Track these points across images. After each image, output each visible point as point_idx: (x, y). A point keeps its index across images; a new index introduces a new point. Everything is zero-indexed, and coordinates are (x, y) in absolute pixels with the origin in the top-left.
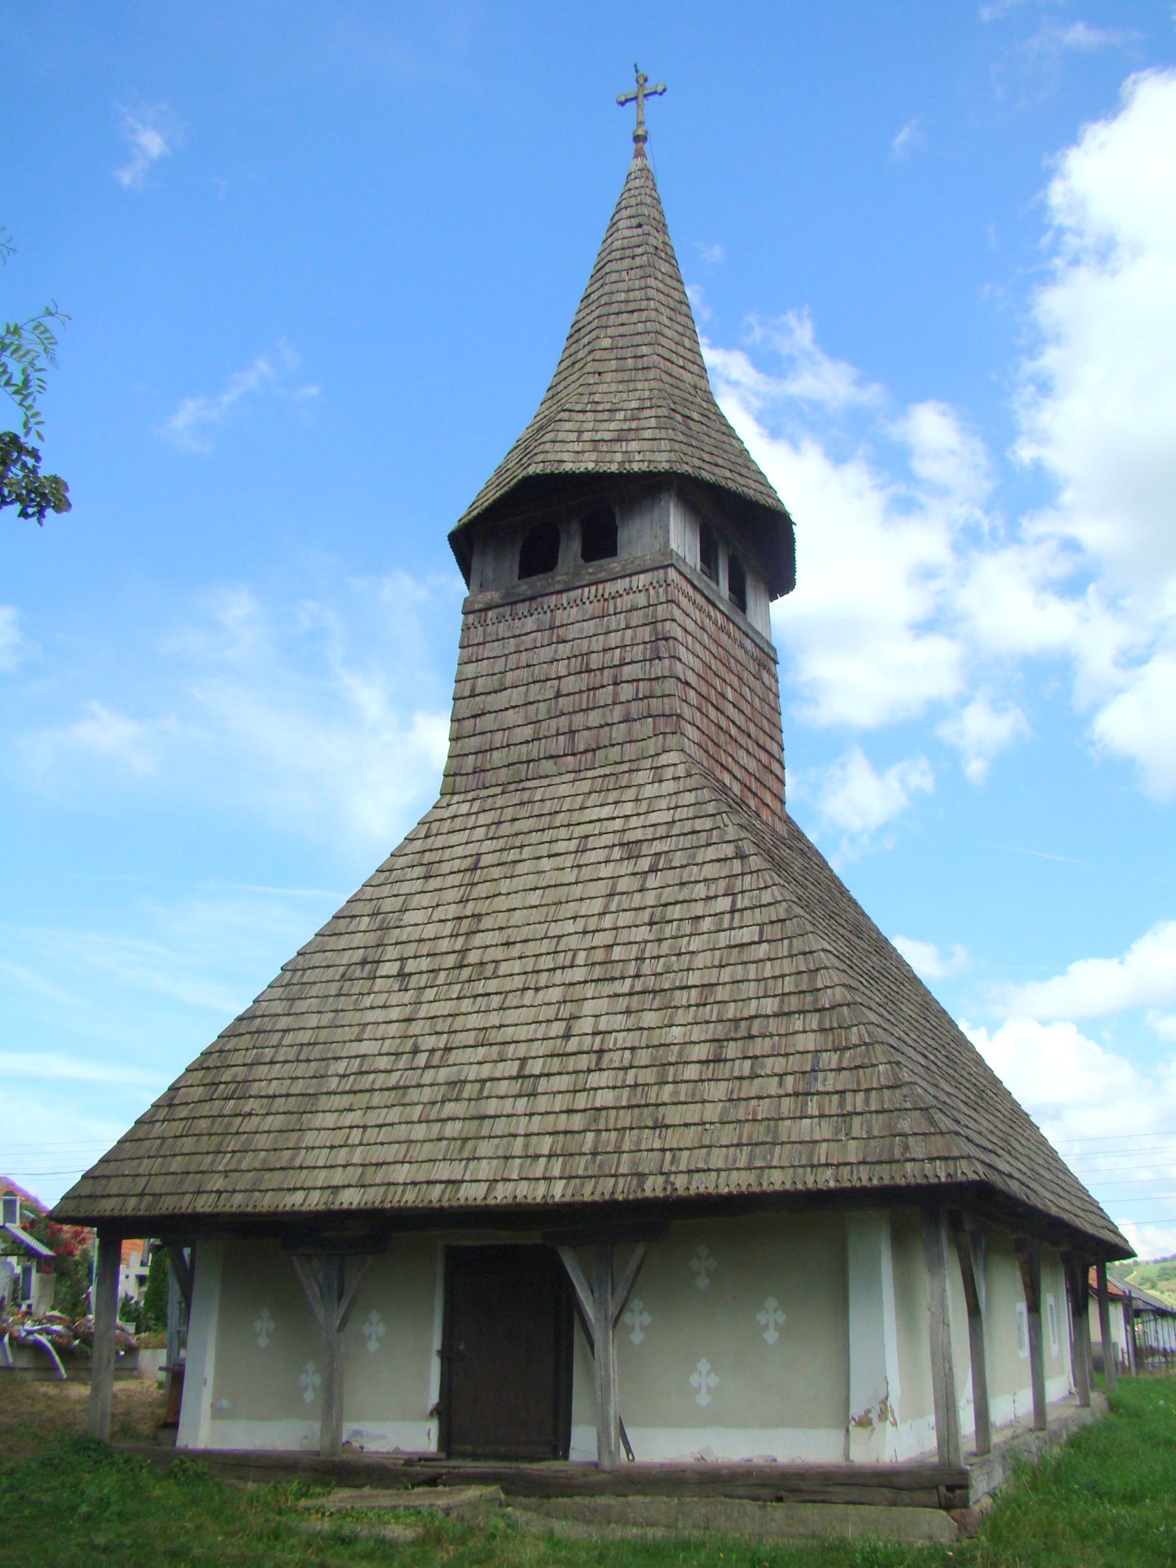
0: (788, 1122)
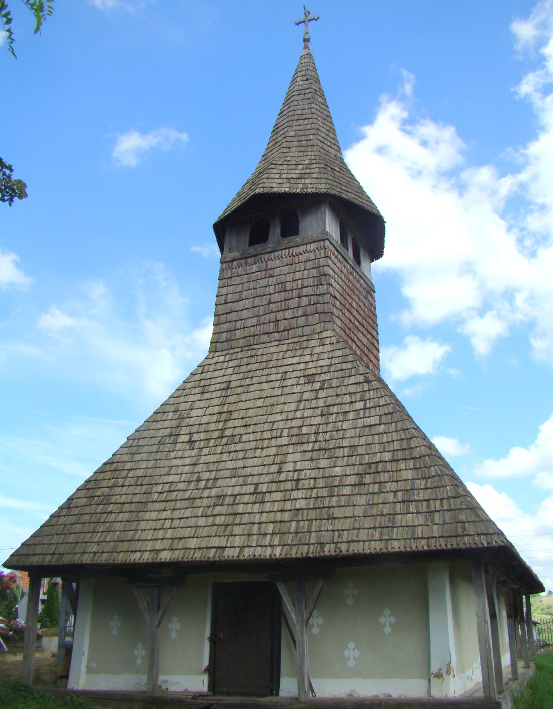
0: (400, 516)
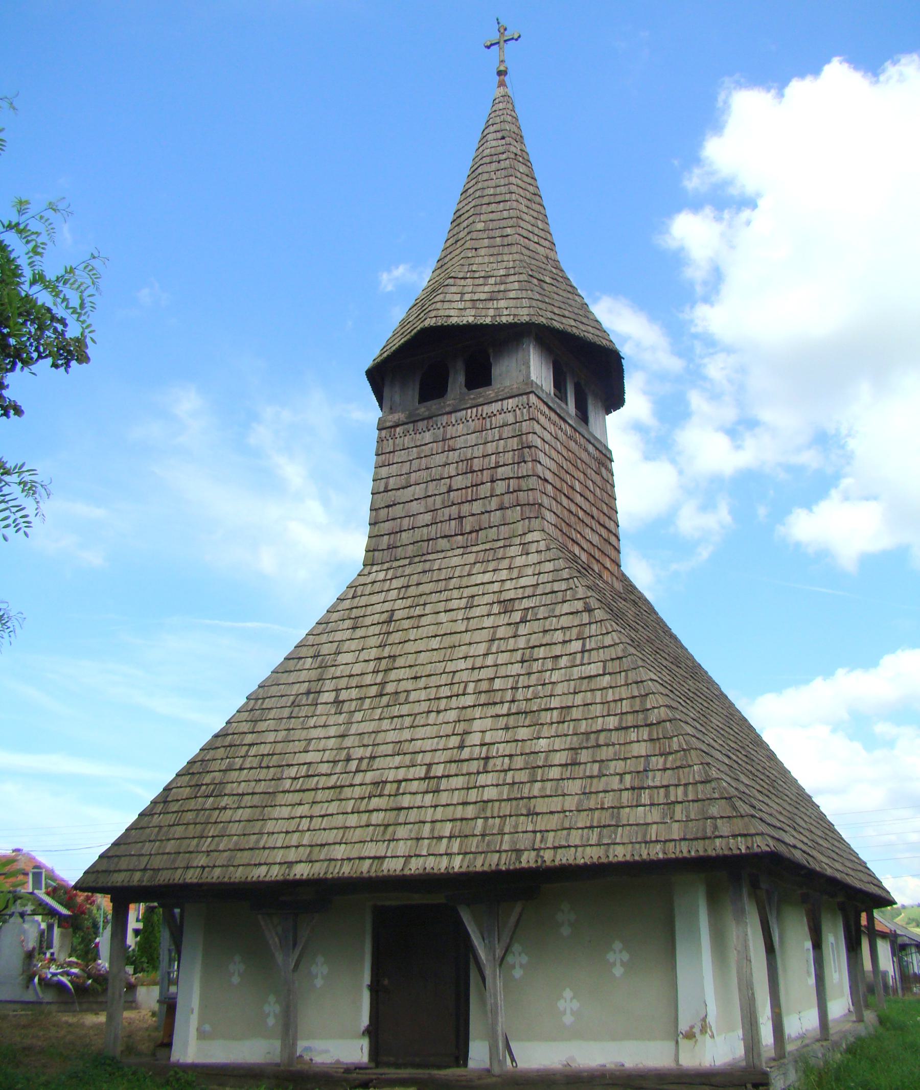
0: (627, 810)
